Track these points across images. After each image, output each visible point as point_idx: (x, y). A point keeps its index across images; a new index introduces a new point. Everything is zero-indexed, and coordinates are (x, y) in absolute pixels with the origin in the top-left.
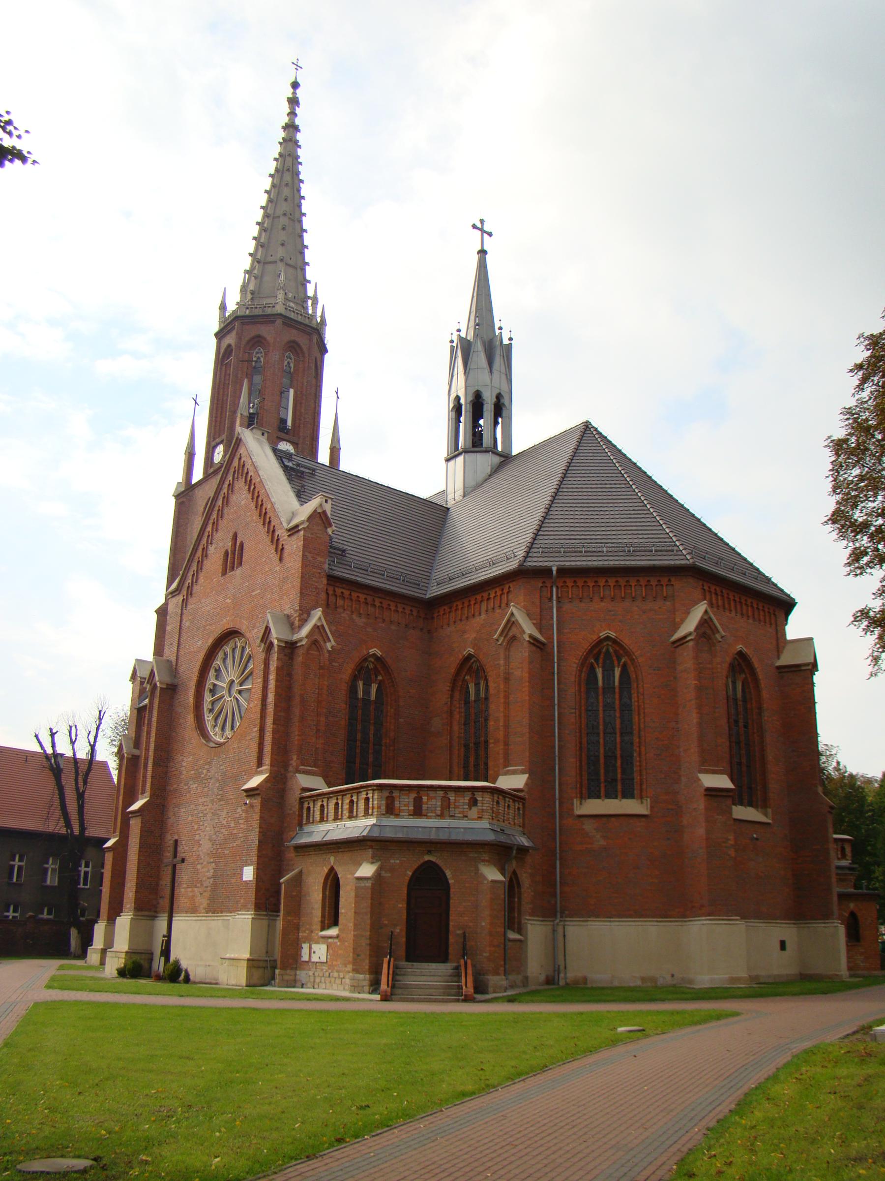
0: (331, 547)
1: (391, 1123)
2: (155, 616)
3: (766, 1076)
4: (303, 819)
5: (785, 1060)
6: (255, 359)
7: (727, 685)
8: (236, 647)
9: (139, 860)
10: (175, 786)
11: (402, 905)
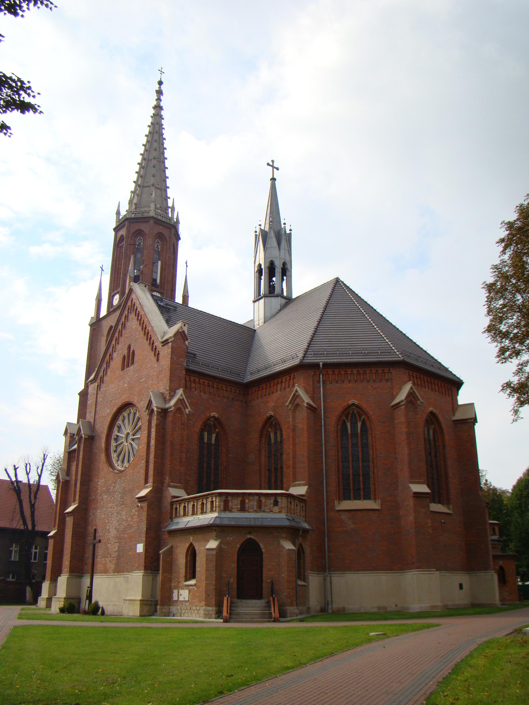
0: (187, 353)
1: (248, 683)
2: (78, 397)
3: (465, 655)
4: (173, 515)
5: (475, 647)
6: (137, 243)
7: (424, 432)
8: (130, 413)
9: (72, 542)
10: (94, 497)
11: (234, 565)
